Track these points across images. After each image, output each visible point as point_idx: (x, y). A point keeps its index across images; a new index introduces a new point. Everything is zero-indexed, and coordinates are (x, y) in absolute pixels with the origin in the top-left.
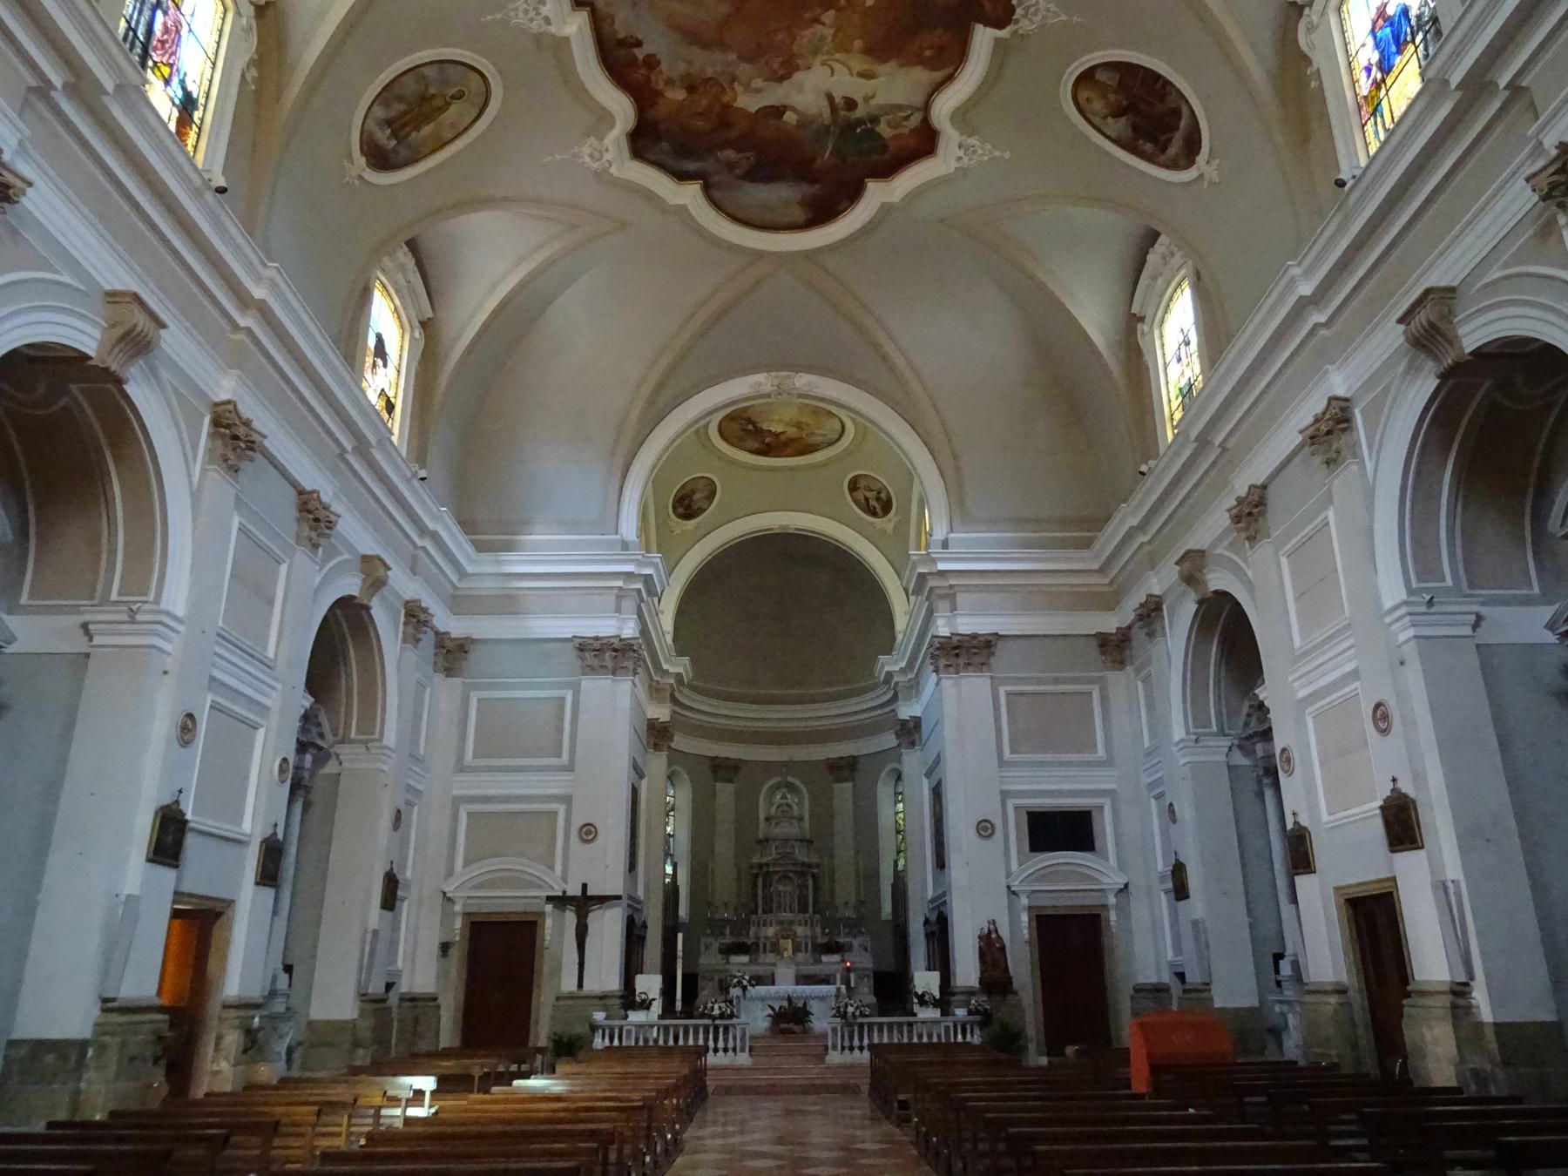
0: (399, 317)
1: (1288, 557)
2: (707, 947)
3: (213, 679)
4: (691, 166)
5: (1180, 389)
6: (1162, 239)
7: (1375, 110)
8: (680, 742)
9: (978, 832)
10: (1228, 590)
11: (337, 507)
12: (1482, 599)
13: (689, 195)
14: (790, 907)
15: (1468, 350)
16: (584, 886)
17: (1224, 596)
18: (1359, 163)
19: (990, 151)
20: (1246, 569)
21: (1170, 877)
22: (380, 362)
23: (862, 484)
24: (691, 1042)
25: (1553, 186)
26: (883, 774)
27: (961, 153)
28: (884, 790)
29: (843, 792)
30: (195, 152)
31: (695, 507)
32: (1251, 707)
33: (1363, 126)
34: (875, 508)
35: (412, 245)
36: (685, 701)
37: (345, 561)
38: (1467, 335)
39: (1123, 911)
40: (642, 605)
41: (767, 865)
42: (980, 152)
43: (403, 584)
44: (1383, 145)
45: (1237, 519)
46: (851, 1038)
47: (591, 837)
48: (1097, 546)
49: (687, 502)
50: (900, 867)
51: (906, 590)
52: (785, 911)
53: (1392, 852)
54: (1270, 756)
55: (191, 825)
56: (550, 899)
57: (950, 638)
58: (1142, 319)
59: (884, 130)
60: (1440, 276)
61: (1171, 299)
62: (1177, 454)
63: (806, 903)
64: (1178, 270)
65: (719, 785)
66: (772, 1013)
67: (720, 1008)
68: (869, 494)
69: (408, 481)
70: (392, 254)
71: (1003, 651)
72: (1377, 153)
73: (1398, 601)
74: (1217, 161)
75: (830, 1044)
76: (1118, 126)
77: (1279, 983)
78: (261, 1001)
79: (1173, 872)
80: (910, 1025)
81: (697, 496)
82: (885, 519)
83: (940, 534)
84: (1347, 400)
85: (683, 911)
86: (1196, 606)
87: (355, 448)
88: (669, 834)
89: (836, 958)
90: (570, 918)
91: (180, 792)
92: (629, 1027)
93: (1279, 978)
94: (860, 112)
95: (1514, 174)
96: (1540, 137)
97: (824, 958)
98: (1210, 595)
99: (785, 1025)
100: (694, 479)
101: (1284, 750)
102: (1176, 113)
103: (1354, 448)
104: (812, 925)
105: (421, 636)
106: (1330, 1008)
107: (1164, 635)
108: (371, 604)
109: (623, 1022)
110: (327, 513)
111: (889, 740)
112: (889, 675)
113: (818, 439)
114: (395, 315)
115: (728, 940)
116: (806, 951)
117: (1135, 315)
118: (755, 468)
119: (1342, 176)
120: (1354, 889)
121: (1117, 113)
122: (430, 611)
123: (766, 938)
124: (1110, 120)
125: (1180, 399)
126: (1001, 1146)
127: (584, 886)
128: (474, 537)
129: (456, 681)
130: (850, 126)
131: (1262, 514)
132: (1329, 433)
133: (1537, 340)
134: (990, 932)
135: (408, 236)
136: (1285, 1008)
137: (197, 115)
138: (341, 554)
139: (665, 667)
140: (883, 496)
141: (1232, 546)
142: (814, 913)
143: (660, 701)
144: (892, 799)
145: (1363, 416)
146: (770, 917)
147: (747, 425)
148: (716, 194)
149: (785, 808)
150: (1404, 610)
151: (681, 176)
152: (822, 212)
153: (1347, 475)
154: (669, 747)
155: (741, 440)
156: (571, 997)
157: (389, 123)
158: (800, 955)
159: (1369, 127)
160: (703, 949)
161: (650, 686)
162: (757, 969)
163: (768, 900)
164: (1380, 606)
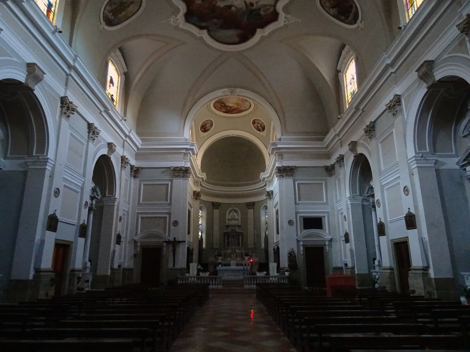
0: (117, 71)
1: (381, 143)
3: (64, 178)
4: (204, 24)
5: (351, 93)
6: (347, 46)
7: (412, 5)
8: (203, 197)
10: (362, 153)
11: (99, 128)
12: (438, 156)
13: (204, 34)
15: (437, 80)
16: (175, 238)
17: (362, 155)
18: (406, 22)
19: (294, 19)
20: (368, 147)
21: (344, 237)
22: (111, 85)
23: (256, 122)
24: (205, 282)
25: (464, 28)
26: (262, 207)
27: (285, 20)
28: (262, 212)
29: (251, 211)
30: (53, 21)
31: (207, 129)
32: (369, 188)
33: (408, 10)
34: (260, 129)
35: (121, 49)
37: (103, 144)
38: (437, 75)
39: (330, 246)
40: (191, 157)
42: (291, 19)
43: (119, 151)
44: (414, 15)
45: (366, 132)
46: (251, 281)
48: (325, 140)
49: (204, 127)
50: (267, 234)
51: (269, 153)
52: (233, 246)
53: (408, 229)
54: (373, 202)
55: (59, 220)
56: (165, 242)
57: (281, 167)
58: (340, 71)
59: (262, 13)
60: (430, 57)
61: (349, 65)
62: (349, 113)
64: (351, 56)
65: (214, 210)
68: (258, 125)
69: (121, 121)
70: (115, 52)
72: (412, 18)
73: (412, 156)
74: (364, 22)
75: (245, 283)
76: (333, 11)
77: (374, 267)
78: (82, 270)
79: (345, 235)
81: (207, 125)
82: (263, 132)
83: (279, 136)
84: (400, 96)
86: (354, 158)
87: (104, 111)
88: (200, 224)
90: (171, 248)
91: (56, 210)
93: (375, 265)
94: (255, 6)
95: (453, 24)
96: (462, 12)
98: (358, 155)
100: (207, 120)
101: (377, 200)
102: (351, 7)
103: (401, 110)
105: (126, 166)
106: (388, 274)
107: (344, 166)
108: (111, 157)
110: (96, 130)
111: (264, 197)
112: (264, 178)
113: (243, 108)
114: (116, 71)
117: (338, 70)
118: (224, 117)
119: (401, 26)
120: (396, 240)
121: (333, 7)
122: (129, 159)
124: (331, 9)
125: (351, 96)
126: (289, 311)
127: (175, 238)
128: (142, 137)
129: (138, 180)
130: (252, 11)
131: (374, 130)
132: (394, 105)
133: (458, 77)
135: (119, 46)
136: (376, 274)
137: (53, 9)
138: (102, 142)
139: (198, 176)
140: (262, 125)
141: (365, 140)
143: (197, 186)
144: (265, 214)
145: (404, 100)
147: (222, 104)
148: (211, 33)
150: (414, 159)
151: (201, 28)
152: (244, 39)
153: (399, 119)
154: (200, 199)
156: (171, 269)
157: (111, 11)
159: (410, 11)
161: (194, 181)
164: (407, 158)
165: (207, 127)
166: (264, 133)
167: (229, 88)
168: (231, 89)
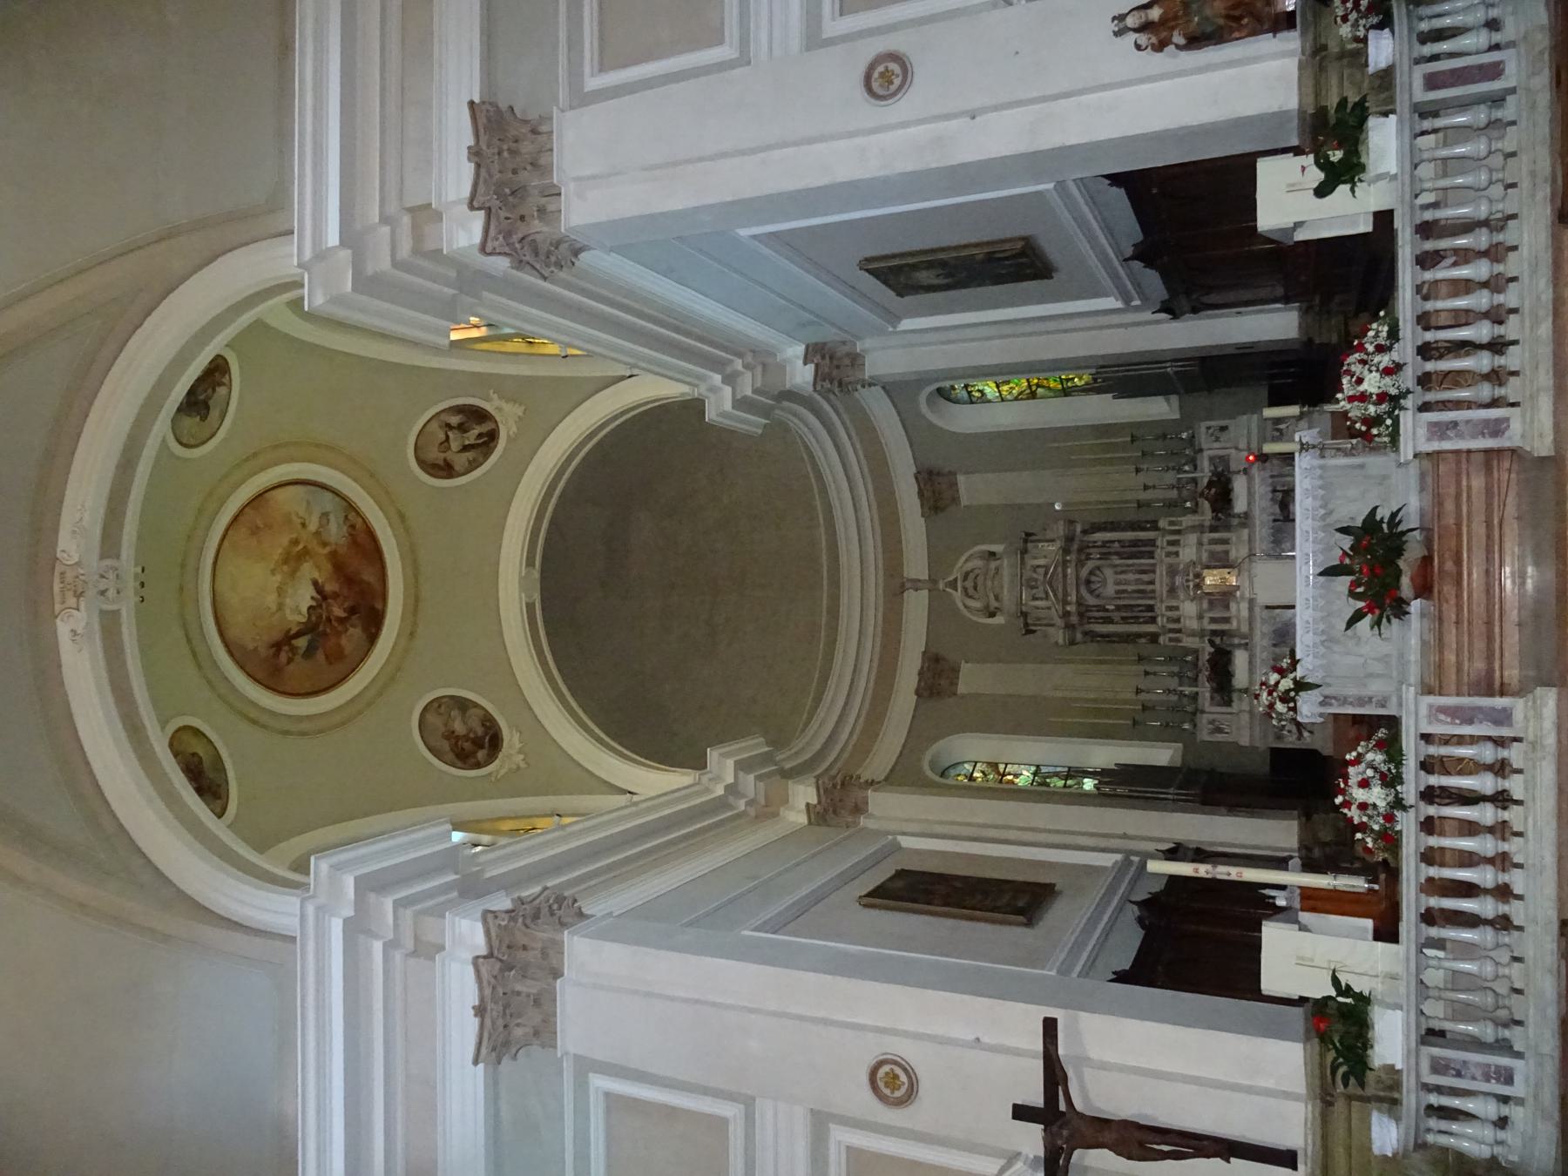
2: (1219, 730)
9: (894, 94)
14: (1144, 572)
16: (1022, 1113)
23: (434, 455)
28: (963, 420)
29: (973, 489)
31: (480, 731)
34: (480, 436)
36: (817, 746)
41: (1066, 614)
47: (903, 1078)
52: (1152, 582)
63: (1135, 543)
65: (962, 688)
66: (1368, 619)
67: (1364, 784)
68: (455, 445)
71: (518, 96)
80: (1426, 230)
81: (459, 727)
82: (498, 419)
85: (1161, 755)
89: (1239, 485)
92: (1425, 1065)
97: (1240, 505)
99: (1405, 581)
104: (1178, 532)
109: (1409, 1083)
115: (1205, 690)
116: (1225, 542)
123: (1200, 617)
127: (1022, 1113)
134: (1144, 28)
140: (455, 420)
142: (1156, 528)
146: (1161, 608)
149: (969, 584)
155: (335, 656)
158: (1238, 552)
160: (1219, 737)
162: (1261, 641)
163: (1131, 613)
165: (470, 730)
166: (499, 409)
167: (58, 607)
168: (62, 591)
